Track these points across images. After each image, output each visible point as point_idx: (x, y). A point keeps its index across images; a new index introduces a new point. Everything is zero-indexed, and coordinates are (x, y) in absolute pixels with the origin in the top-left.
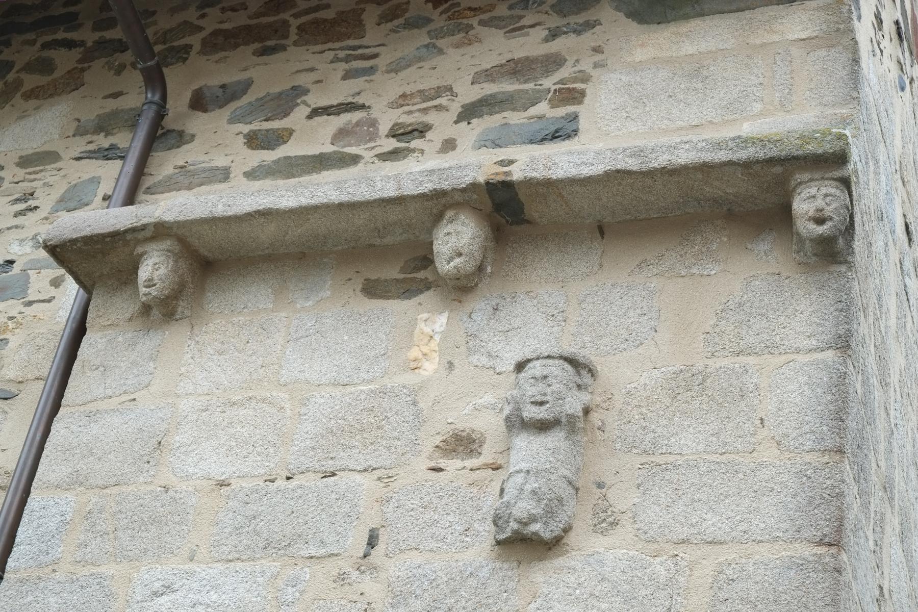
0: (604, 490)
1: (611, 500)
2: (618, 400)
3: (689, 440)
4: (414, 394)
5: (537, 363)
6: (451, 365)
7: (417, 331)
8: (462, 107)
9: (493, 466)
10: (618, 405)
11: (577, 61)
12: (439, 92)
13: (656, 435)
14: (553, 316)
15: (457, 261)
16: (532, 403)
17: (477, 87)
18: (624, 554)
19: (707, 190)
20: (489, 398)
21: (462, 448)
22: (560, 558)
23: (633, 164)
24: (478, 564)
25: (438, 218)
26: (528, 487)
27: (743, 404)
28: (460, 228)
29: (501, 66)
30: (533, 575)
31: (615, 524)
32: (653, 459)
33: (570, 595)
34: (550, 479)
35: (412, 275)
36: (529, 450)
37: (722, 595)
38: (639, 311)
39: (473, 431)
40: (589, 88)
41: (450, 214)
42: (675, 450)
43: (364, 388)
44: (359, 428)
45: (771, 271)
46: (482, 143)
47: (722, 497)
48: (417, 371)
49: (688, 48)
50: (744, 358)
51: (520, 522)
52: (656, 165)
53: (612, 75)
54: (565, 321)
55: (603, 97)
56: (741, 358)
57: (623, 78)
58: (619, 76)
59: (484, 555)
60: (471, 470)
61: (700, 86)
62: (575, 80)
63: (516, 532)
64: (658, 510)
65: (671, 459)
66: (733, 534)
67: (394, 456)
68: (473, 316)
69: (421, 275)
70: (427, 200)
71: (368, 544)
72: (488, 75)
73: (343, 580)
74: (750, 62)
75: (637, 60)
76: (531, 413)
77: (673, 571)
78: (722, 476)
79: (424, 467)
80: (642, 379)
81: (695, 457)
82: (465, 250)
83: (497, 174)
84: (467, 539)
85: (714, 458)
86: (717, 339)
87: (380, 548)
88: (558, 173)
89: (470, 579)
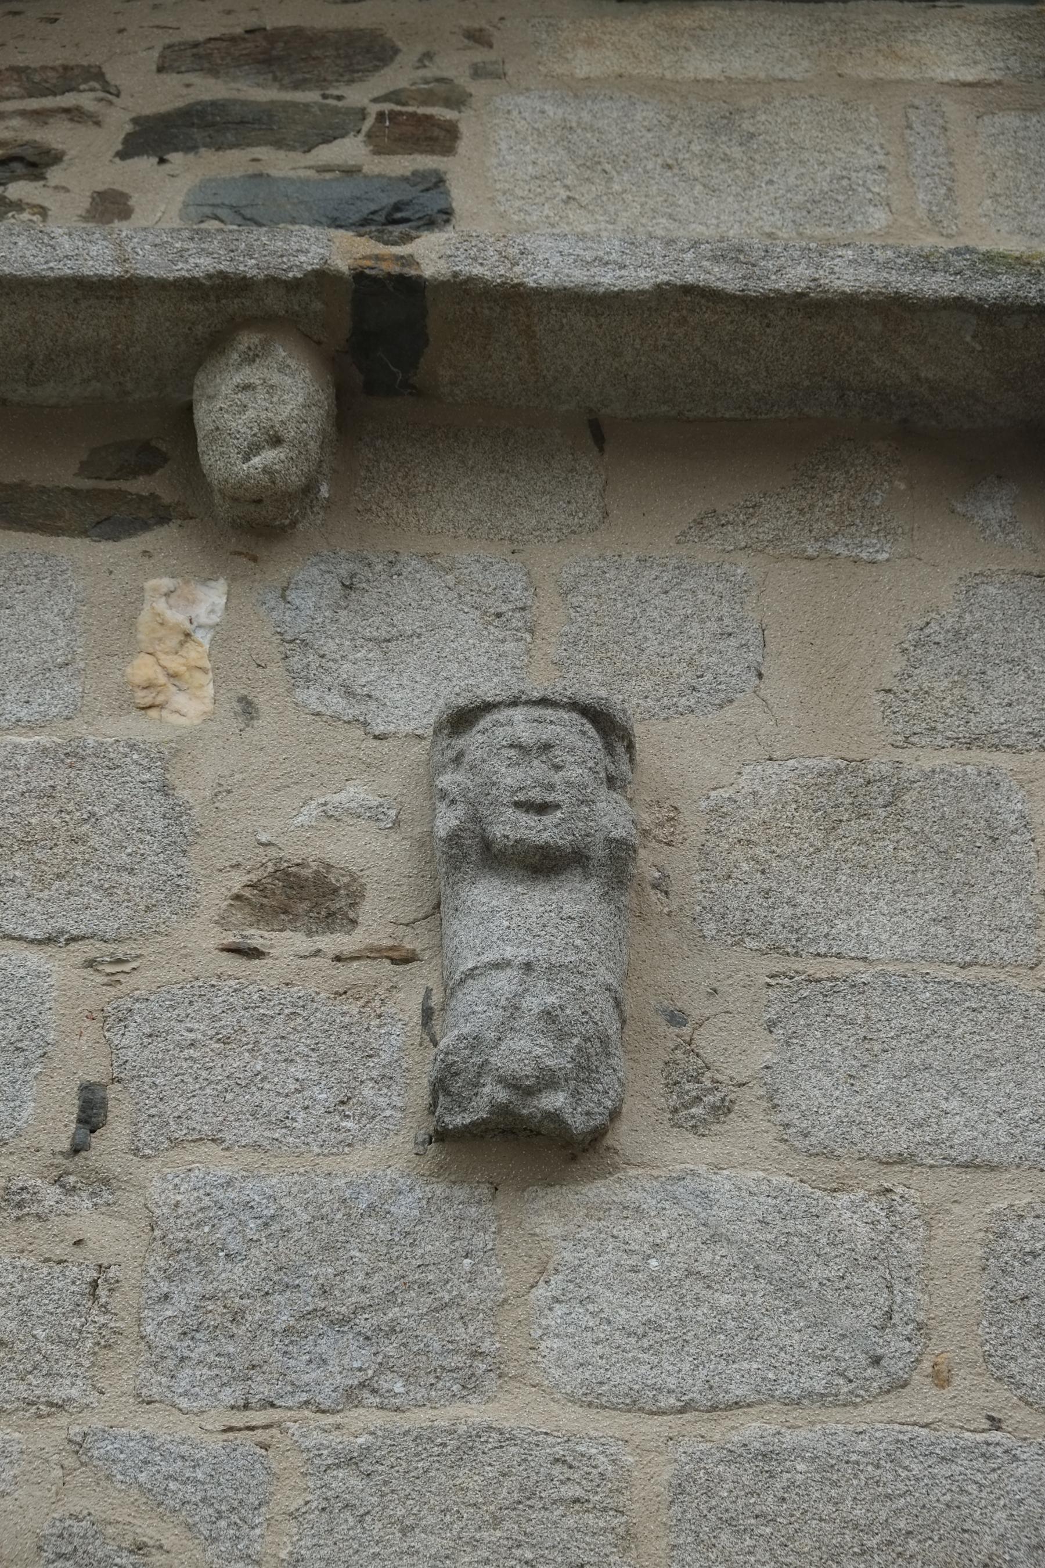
0: (687, 1030)
1: (708, 1054)
2: (693, 824)
3: (882, 926)
4: (165, 763)
5: (518, 714)
6: (248, 709)
7: (145, 617)
8: (135, 121)
9: (395, 954)
10: (696, 837)
11: (428, 56)
12: (69, 78)
13: (799, 911)
14: (499, 615)
15: (269, 456)
16: (517, 805)
17: (172, 80)
18: (758, 1182)
19: (878, 364)
20: (356, 793)
21: (305, 905)
22: (599, 1183)
23: (724, 277)
24: (387, 1186)
25: (212, 345)
26: (532, 1004)
27: (998, 858)
28: (276, 378)
29: (233, 39)
30: (535, 1219)
31: (723, 1110)
32: (795, 967)
33: (634, 1270)
34: (581, 989)
35: (114, 485)
36: (503, 921)
37: (1013, 1286)
38: (712, 626)
39: (329, 867)
40: (467, 122)
41: (248, 340)
42: (849, 947)
43: (24, 740)
44: (19, 835)
45: (1022, 567)
46: (207, 210)
47: (979, 1064)
48: (153, 713)
49: (701, 65)
50: (984, 754)
51: (513, 1084)
52: (781, 285)
53: (520, 99)
54: (532, 631)
55: (504, 146)
56: (975, 755)
57: (550, 109)
58: (538, 104)
59: (400, 1164)
60: (338, 959)
61: (736, 152)
62: (429, 98)
63: (501, 1110)
64: (827, 1083)
65: (842, 968)
66: (1019, 1149)
67: (124, 912)
68: (291, 595)
69: (139, 485)
70: (192, 299)
71: (80, 1121)
72: (201, 56)
73: (20, 1205)
74: (849, 115)
75: (581, 72)
76: (511, 827)
77: (884, 1226)
78: (972, 1015)
79: (212, 943)
80: (742, 781)
81: (901, 968)
82: (290, 433)
83: (378, 258)
84: (348, 1124)
85: (947, 972)
86: (913, 707)
87: (115, 1134)
88: (540, 274)
89: (367, 1221)
